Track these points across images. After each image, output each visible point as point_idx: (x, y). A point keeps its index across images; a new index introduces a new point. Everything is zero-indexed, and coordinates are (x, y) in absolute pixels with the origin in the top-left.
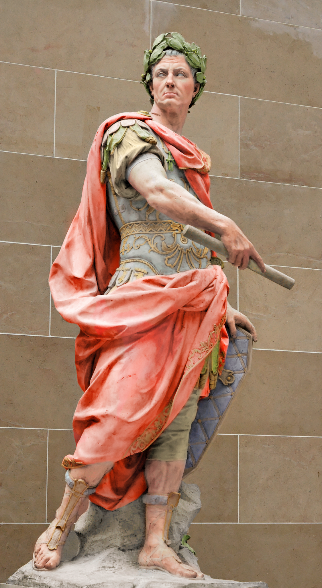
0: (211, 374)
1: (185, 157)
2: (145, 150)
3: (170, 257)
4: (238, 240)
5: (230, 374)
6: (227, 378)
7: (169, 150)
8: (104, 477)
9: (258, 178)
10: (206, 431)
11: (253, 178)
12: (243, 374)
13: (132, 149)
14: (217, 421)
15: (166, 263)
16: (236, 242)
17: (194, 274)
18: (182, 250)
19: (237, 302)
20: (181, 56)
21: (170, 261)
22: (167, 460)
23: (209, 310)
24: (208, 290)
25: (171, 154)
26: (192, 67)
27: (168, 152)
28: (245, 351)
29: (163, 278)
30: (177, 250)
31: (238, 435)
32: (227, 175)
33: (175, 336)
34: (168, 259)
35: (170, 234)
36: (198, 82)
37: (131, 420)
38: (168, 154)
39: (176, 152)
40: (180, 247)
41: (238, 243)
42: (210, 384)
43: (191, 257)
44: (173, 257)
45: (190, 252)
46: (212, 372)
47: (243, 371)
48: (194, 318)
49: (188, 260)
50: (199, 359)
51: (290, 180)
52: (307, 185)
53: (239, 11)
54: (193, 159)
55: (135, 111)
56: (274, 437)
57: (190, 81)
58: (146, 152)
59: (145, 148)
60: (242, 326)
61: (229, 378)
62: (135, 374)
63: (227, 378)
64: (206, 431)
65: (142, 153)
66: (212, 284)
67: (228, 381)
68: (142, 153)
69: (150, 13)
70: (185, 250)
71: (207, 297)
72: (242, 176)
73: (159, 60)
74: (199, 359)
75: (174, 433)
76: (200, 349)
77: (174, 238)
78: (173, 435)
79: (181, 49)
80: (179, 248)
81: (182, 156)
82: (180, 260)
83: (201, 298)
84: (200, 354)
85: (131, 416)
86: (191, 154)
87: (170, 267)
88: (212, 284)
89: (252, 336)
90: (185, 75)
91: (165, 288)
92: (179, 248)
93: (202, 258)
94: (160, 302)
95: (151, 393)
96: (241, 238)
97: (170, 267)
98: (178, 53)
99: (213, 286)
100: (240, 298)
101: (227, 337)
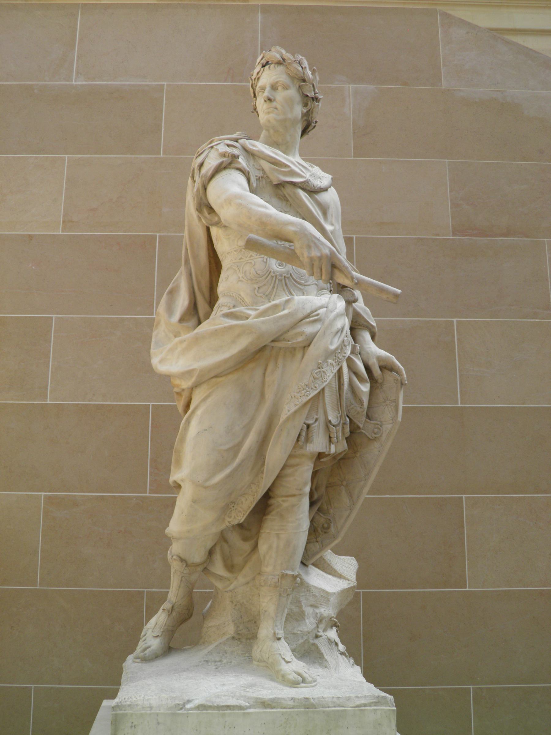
0: (329, 424)
1: (277, 170)
2: (223, 166)
3: (261, 285)
4: (312, 245)
5: (376, 426)
6: (373, 432)
7: (260, 166)
8: (211, 553)
9: (471, 235)
10: (350, 495)
11: (466, 236)
12: (391, 425)
13: (210, 166)
14: (362, 483)
15: (256, 293)
16: (309, 247)
17: (288, 301)
18: (276, 276)
19: (455, 359)
20: (281, 68)
21: (261, 290)
22: (277, 532)
23: (312, 344)
24: (308, 320)
25: (263, 170)
26: (292, 78)
27: (258, 168)
28: (393, 398)
29: (248, 309)
30: (270, 276)
31: (464, 496)
32: (438, 235)
33: (267, 379)
34: (259, 288)
35: (262, 259)
36: (307, 96)
37: (207, 484)
38: (259, 170)
39: (266, 166)
40: (274, 272)
41: (313, 248)
42: (330, 437)
43: (288, 283)
44: (265, 285)
45: (288, 278)
46: (330, 421)
47: (391, 421)
48: (293, 355)
49: (285, 287)
50: (296, 405)
51: (507, 234)
52: (527, 237)
53: (442, 84)
54: (289, 171)
55: (232, 134)
56: (504, 498)
57: (293, 92)
58: (225, 168)
59: (222, 163)
60: (386, 367)
61: (376, 430)
62: (211, 427)
63: (373, 432)
64: (350, 495)
65: (218, 170)
66: (316, 313)
67: (375, 434)
68: (218, 170)
69: (349, 96)
70: (281, 276)
71: (309, 330)
72: (454, 234)
73: (259, 78)
74: (296, 405)
75: (284, 499)
76: (298, 393)
77: (266, 262)
78: (283, 501)
79: (280, 61)
80: (272, 274)
81: (274, 169)
82: (273, 287)
83: (298, 330)
84: (298, 399)
85: (207, 480)
86: (286, 166)
87: (261, 297)
88: (316, 313)
89: (399, 379)
90: (286, 88)
91: (250, 321)
92: (272, 274)
93: (309, 285)
94: (239, 336)
95: (236, 449)
96: (316, 241)
97: (261, 297)
98: (276, 65)
99: (318, 315)
100: (459, 354)
101: (367, 382)
